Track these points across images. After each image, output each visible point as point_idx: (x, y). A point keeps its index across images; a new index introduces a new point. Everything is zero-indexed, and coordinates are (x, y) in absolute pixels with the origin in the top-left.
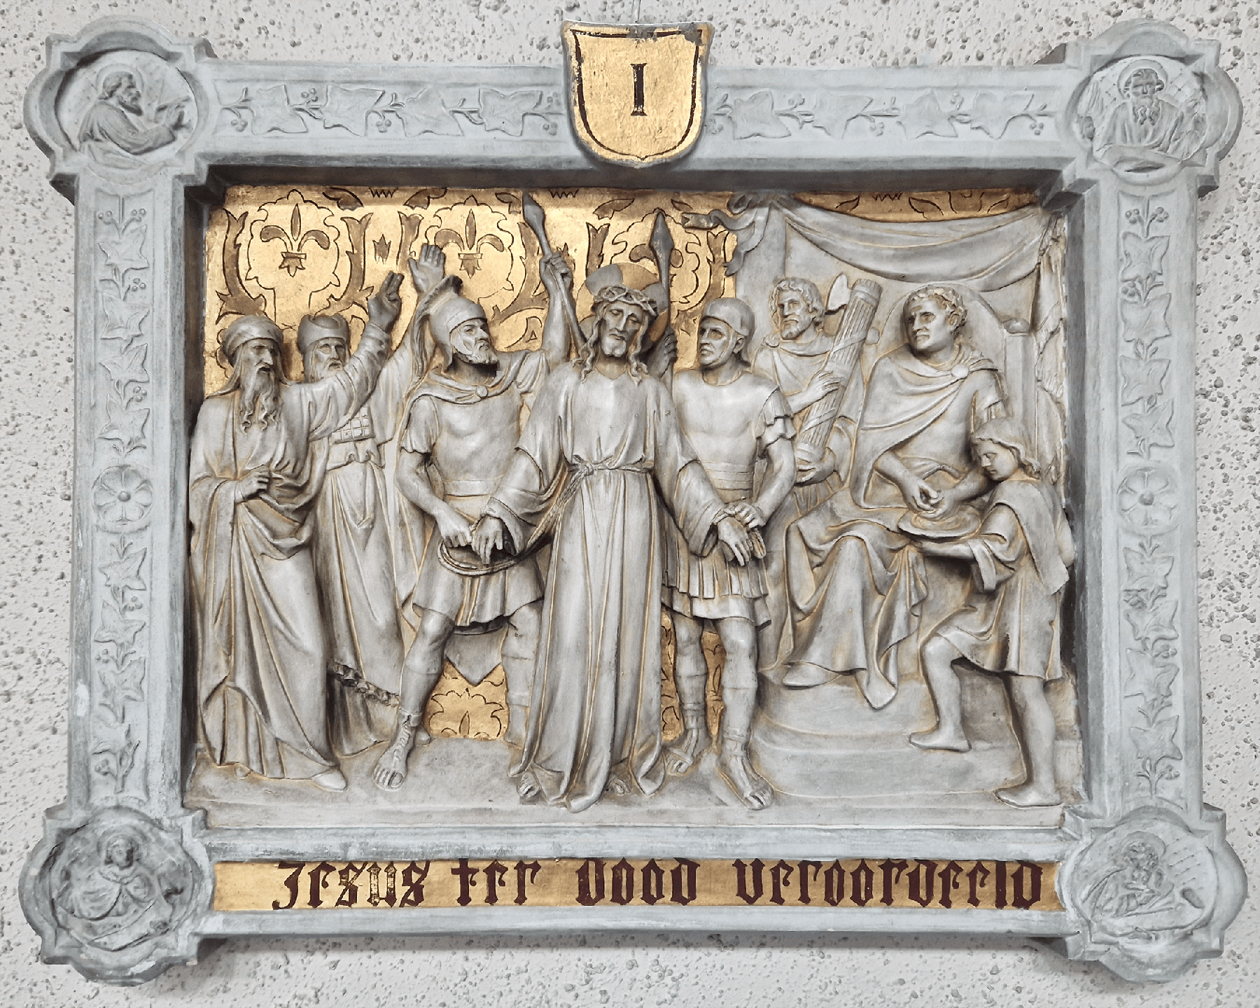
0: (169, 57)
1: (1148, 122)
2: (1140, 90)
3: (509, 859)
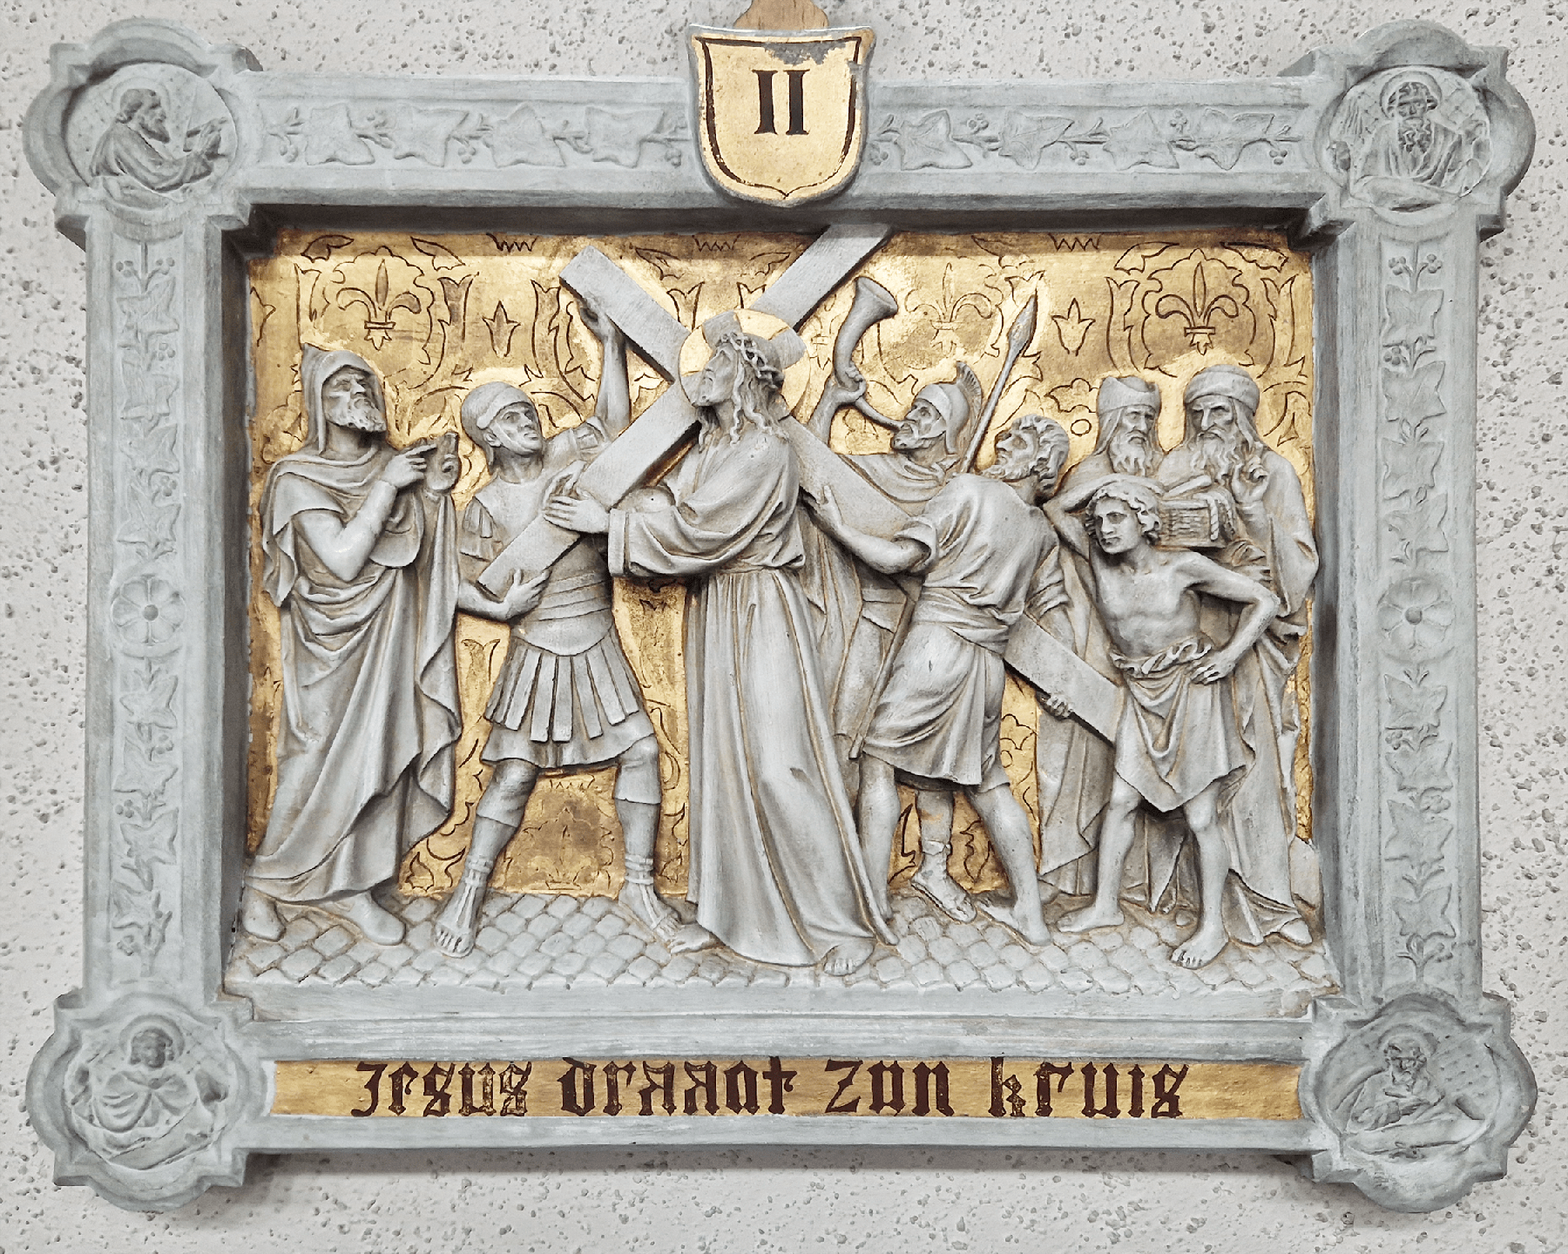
0: (199, 69)
1: (1416, 148)
2: (1407, 109)
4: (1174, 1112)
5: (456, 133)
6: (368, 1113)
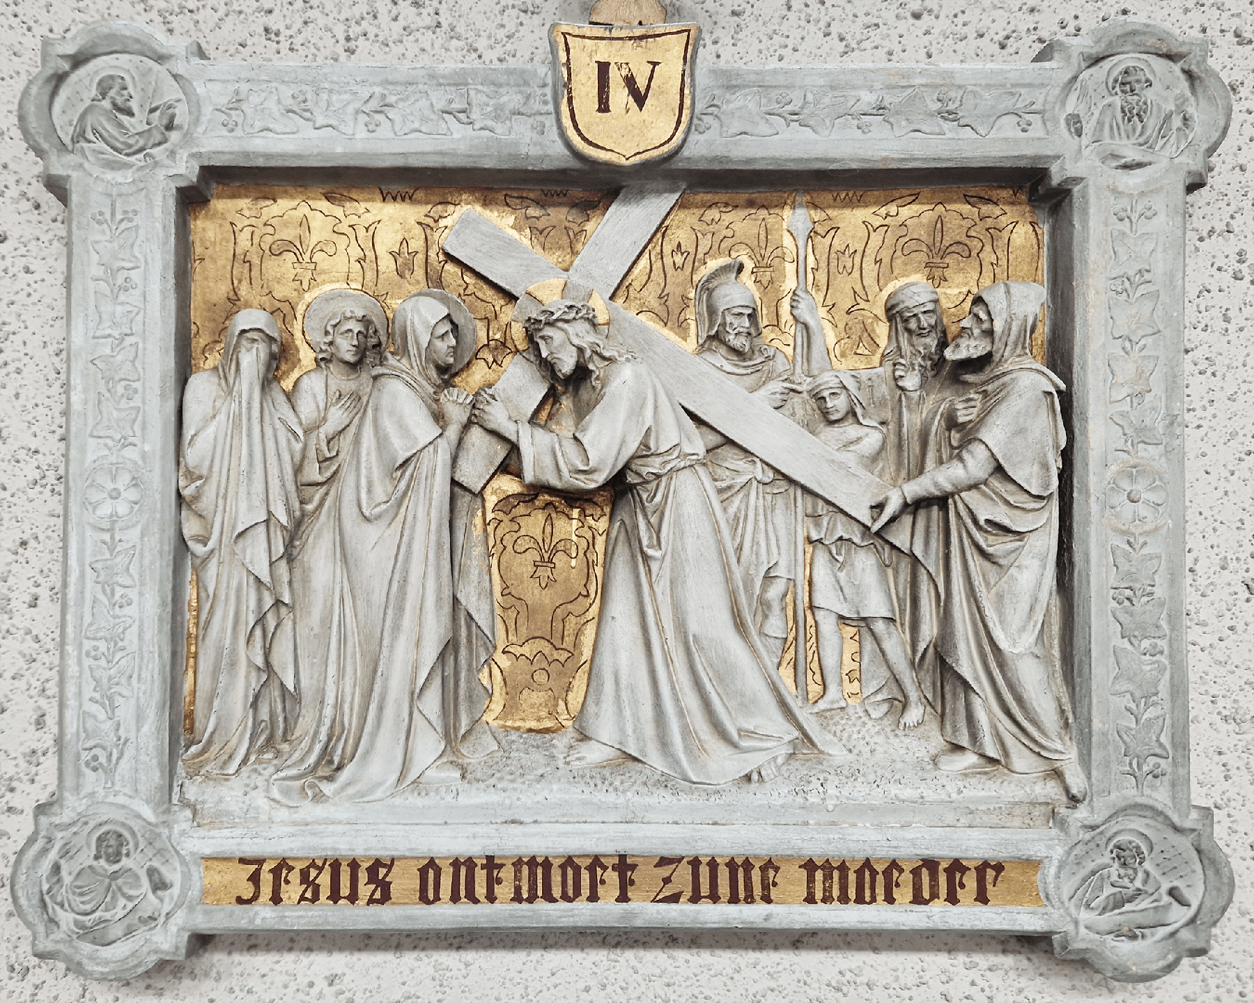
0: (160, 58)
1: (1136, 118)
2: (1128, 88)
3: (506, 857)
4: (386, 898)
6: (249, 902)
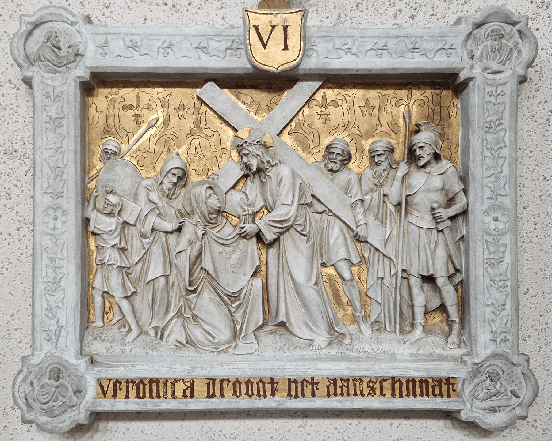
2: (493, 37)
5: (162, 46)
